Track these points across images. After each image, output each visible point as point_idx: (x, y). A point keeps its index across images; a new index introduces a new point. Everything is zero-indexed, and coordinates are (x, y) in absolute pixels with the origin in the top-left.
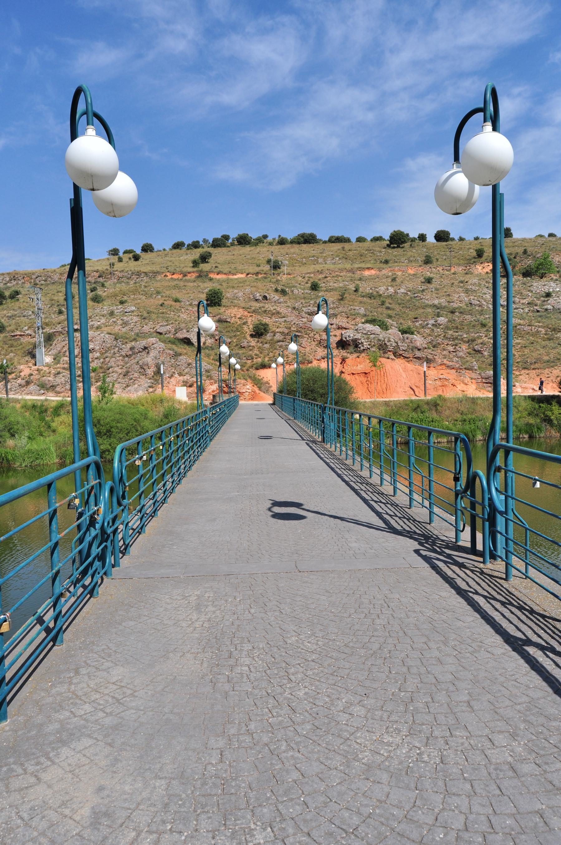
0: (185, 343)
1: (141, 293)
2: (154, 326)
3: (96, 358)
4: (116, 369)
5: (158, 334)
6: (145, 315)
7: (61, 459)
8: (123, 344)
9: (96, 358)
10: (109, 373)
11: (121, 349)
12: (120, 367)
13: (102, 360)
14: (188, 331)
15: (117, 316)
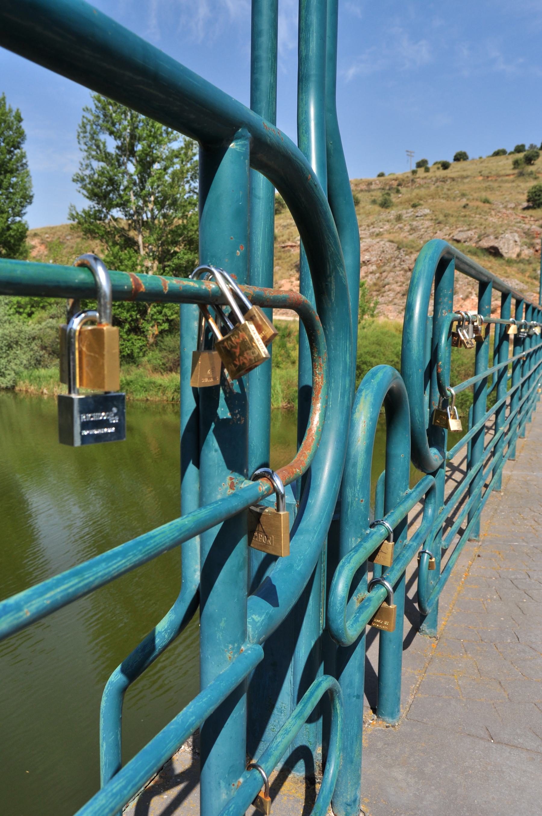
0: (491, 253)
1: (442, 196)
2: (450, 232)
3: (371, 273)
4: (394, 286)
5: (455, 242)
6: (441, 218)
7: (289, 403)
8: (406, 255)
9: (371, 273)
10: (385, 292)
11: (404, 261)
12: (399, 284)
13: (378, 275)
14: (497, 238)
15: (405, 221)
